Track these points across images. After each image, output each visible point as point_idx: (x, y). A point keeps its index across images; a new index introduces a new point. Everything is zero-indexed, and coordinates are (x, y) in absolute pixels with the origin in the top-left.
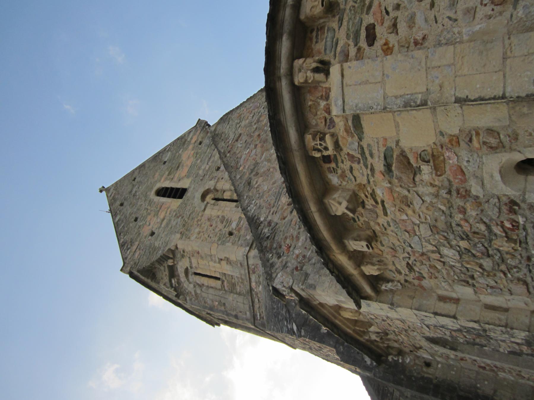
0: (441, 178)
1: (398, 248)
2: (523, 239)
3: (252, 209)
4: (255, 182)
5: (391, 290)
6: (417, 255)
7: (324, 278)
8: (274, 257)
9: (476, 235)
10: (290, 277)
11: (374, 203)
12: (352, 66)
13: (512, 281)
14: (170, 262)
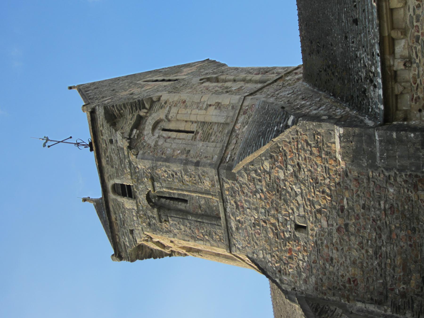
14: (142, 113)
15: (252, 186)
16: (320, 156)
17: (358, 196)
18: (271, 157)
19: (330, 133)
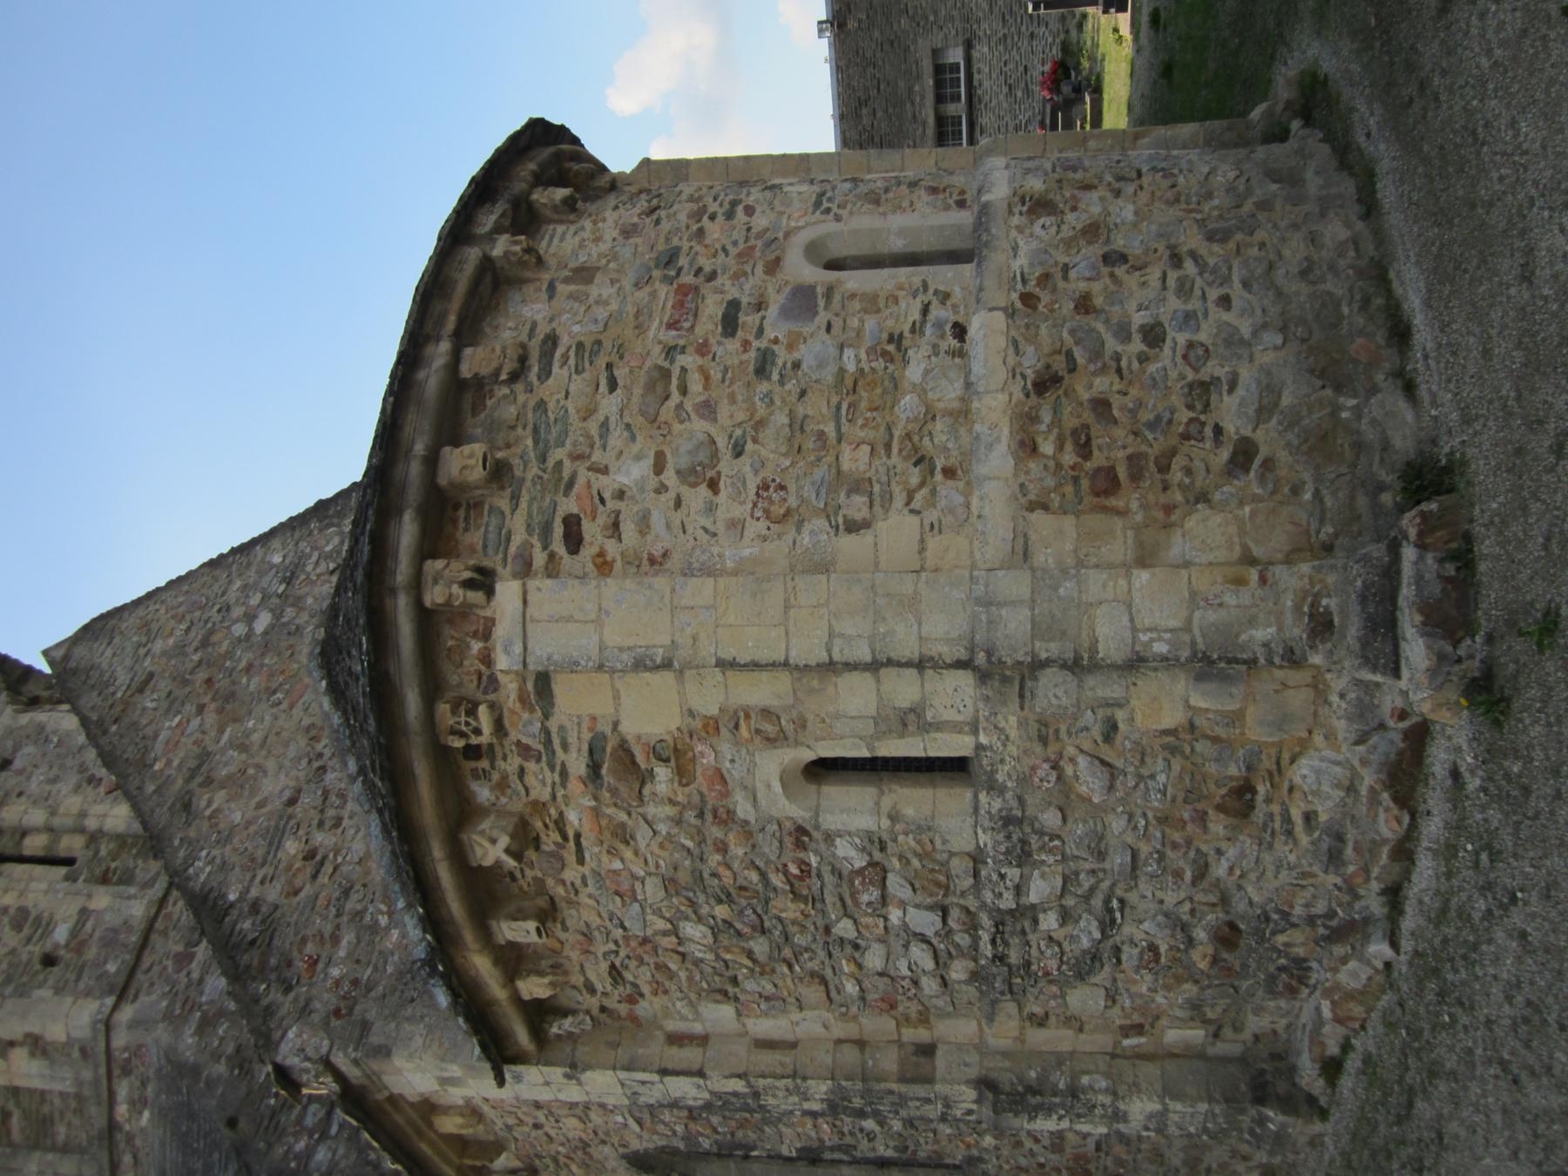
0: (687, 790)
1: (596, 933)
2: (817, 893)
3: (201, 872)
4: (203, 803)
5: (570, 1035)
6: (633, 944)
7: (407, 1027)
8: (273, 990)
9: (743, 893)
10: (322, 1034)
11: (560, 840)
12: (541, 587)
13: (801, 979)
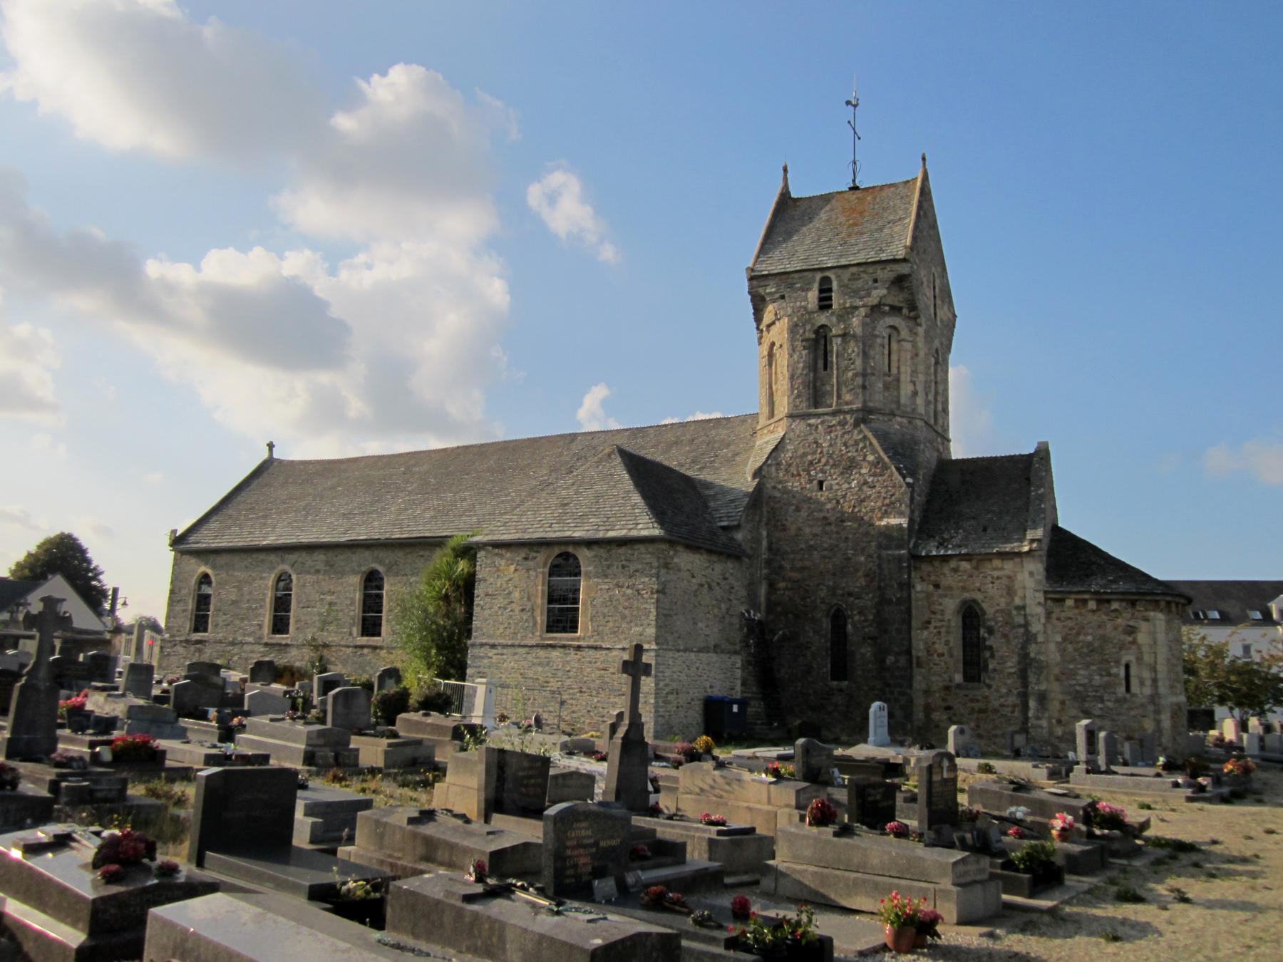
14: (905, 311)
15: (851, 442)
16: (883, 505)
17: (855, 534)
18: (878, 463)
19: (901, 514)
